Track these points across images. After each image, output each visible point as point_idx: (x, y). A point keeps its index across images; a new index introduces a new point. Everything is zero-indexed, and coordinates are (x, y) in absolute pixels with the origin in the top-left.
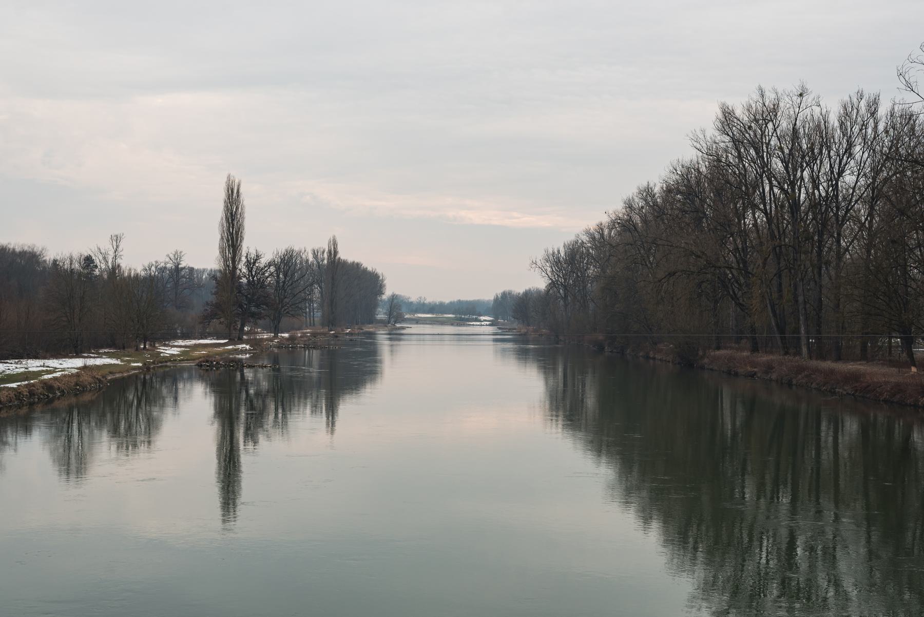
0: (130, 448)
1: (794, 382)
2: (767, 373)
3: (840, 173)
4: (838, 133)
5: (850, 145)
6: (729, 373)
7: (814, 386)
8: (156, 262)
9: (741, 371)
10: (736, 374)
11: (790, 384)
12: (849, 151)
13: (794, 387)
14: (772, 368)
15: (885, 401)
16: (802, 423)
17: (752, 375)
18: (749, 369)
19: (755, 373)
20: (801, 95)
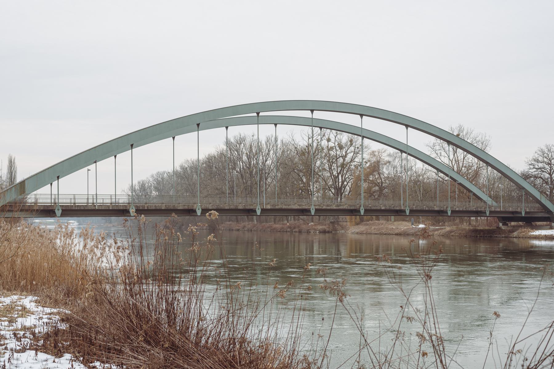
0: (273, 139)
1: (253, 230)
2: (243, 228)
3: (266, 161)
4: (265, 146)
5: (269, 151)
6: (230, 230)
7: (259, 230)
8: (547, 147)
9: (234, 229)
10: (232, 230)
11: (251, 231)
12: (268, 154)
13: (253, 232)
14: (245, 226)
15: (279, 231)
16: (324, 265)
17: (238, 230)
18: (237, 228)
19: (239, 229)
20: (253, 136)
